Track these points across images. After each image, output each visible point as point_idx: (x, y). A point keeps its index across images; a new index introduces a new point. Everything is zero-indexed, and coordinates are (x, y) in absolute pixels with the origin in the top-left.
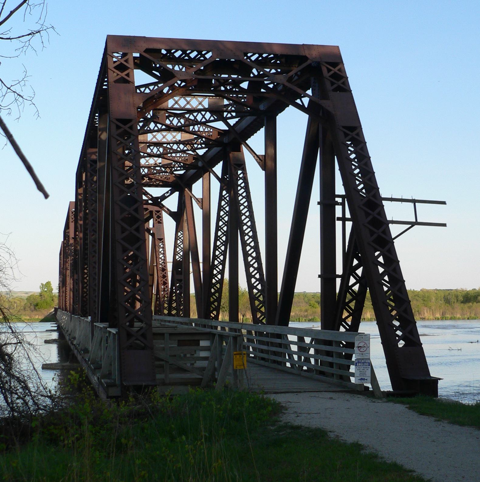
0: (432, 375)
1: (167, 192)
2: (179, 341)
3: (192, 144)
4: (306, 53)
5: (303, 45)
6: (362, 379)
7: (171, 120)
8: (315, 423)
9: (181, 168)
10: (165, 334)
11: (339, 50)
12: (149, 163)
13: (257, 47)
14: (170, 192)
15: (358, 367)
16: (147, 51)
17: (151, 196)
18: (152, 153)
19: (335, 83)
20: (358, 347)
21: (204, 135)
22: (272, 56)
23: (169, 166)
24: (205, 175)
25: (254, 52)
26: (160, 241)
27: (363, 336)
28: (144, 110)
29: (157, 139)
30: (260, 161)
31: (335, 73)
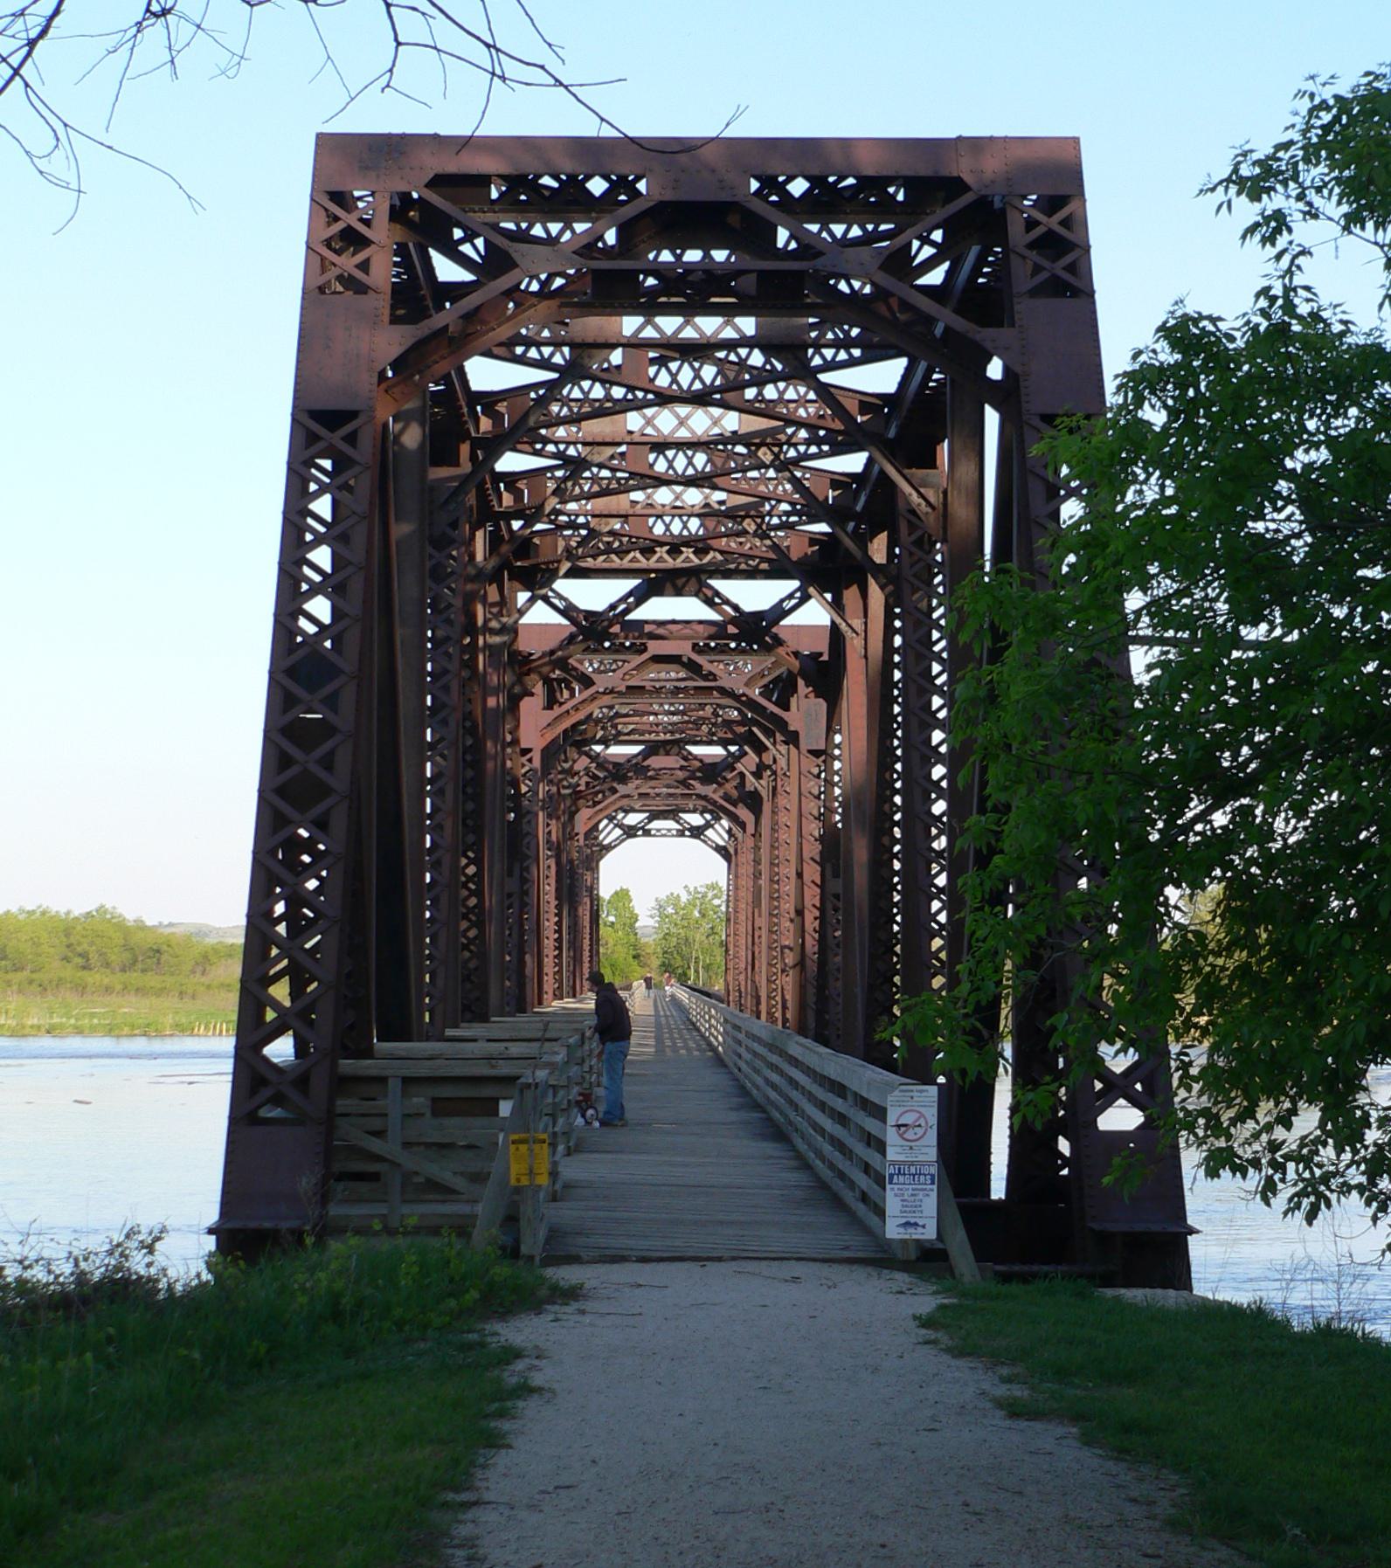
0: (1190, 1221)
1: (791, 596)
2: (434, 1100)
3: (774, 445)
4: (964, 169)
5: (960, 138)
6: (907, 1224)
7: (674, 371)
8: (961, 1363)
9: (800, 517)
10: (390, 1081)
11: (1079, 151)
12: (683, 501)
13: (803, 152)
14: (798, 595)
15: (896, 1187)
16: (439, 182)
17: (736, 608)
18: (671, 472)
19: (1045, 269)
20: (899, 1126)
21: (802, 412)
22: (851, 181)
23: (752, 513)
24: (876, 541)
25: (790, 172)
26: (818, 757)
27: (915, 1094)
28: (417, 377)
29: (657, 430)
30: (929, 510)
31: (1050, 233)
